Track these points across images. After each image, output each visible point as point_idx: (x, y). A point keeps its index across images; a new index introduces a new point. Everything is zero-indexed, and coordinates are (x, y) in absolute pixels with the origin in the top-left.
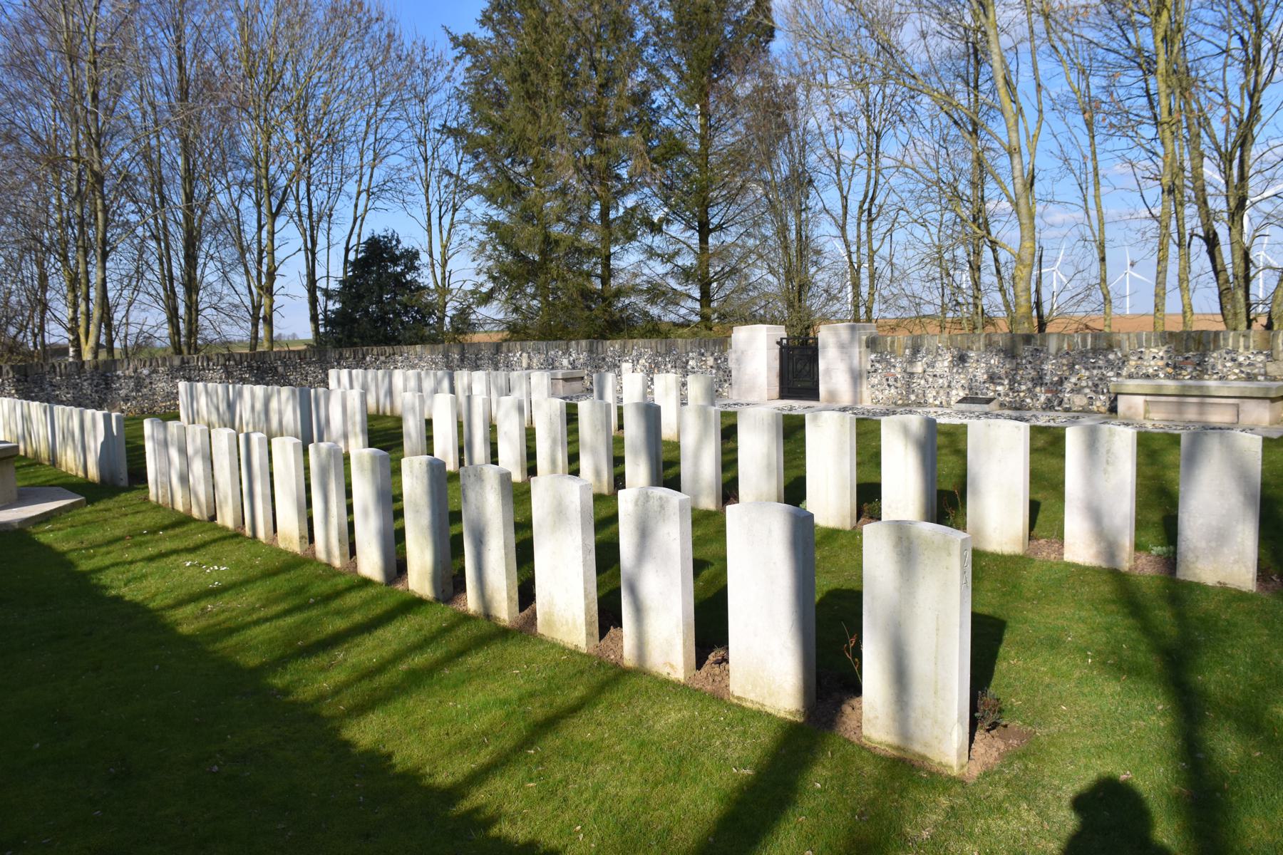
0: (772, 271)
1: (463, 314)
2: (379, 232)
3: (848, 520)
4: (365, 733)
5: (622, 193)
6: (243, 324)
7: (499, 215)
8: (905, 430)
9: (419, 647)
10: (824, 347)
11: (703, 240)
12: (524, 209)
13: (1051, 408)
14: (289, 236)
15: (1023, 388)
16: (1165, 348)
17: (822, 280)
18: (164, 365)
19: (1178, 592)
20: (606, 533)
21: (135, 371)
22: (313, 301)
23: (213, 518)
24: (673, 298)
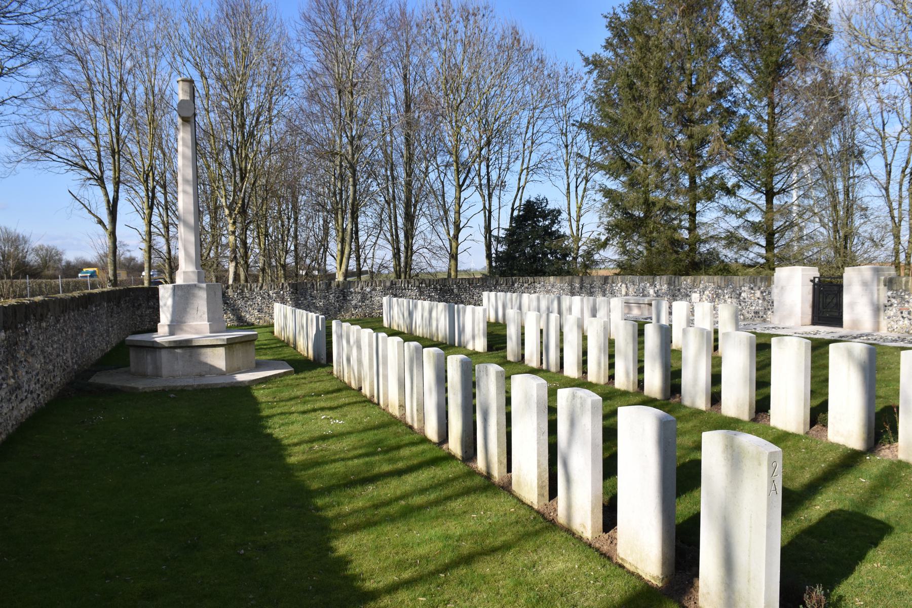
0: (824, 225)
1: (589, 254)
3: (802, 426)
4: (343, 546)
5: (703, 167)
6: (444, 260)
7: (612, 184)
8: (850, 353)
9: (422, 491)
10: (850, 285)
11: (769, 201)
12: (631, 180)
14: (473, 200)
17: (865, 232)
18: (380, 285)
20: (610, 422)
21: (362, 289)
22: (488, 247)
23: (360, 389)
24: (745, 245)
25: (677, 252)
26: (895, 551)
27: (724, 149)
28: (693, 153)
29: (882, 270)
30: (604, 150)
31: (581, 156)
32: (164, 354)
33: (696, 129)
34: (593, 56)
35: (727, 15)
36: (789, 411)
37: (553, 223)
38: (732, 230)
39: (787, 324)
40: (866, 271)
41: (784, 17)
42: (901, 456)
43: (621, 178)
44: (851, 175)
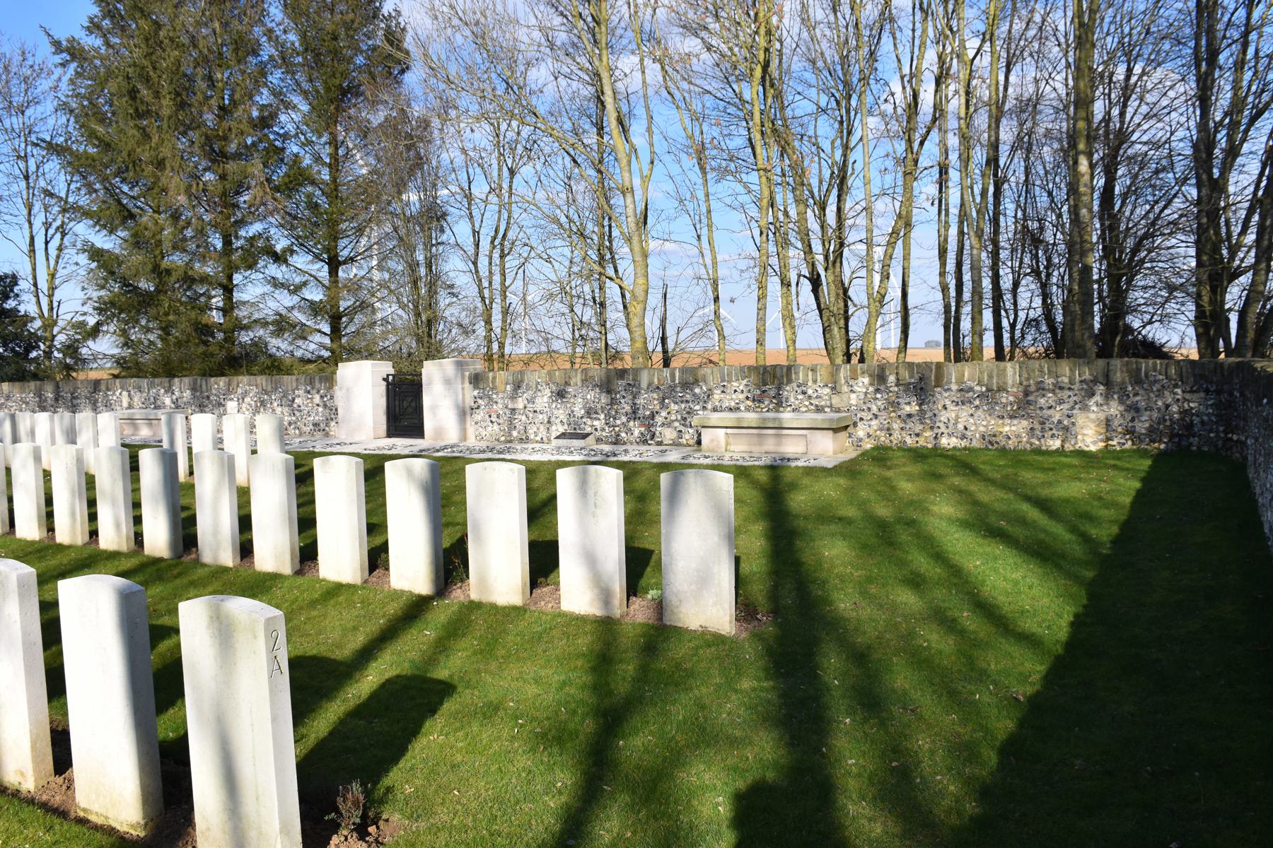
0: (403, 307)
1: (71, 349)
3: (359, 574)
5: (241, 223)
7: (103, 241)
8: (409, 472)
10: (430, 384)
11: (333, 272)
12: (135, 235)
13: (645, 442)
15: (618, 422)
16: (745, 382)
19: (661, 632)
24: (302, 333)
25: (206, 343)
26: (455, 715)
27: (269, 197)
28: (227, 201)
29: (467, 364)
30: (91, 190)
31: (51, 195)
33: (231, 166)
34: (68, 41)
35: (276, 12)
36: (340, 559)
38: (284, 312)
39: (356, 439)
40: (448, 365)
41: (349, 26)
42: (474, 596)
43: (119, 233)
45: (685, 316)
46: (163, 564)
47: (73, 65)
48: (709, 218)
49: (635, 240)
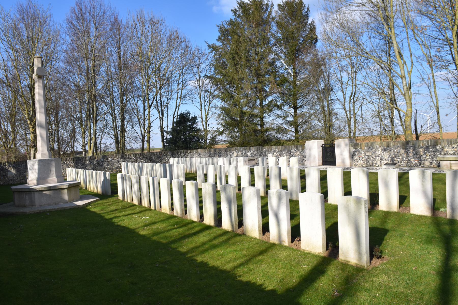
1: (213, 139)
2: (184, 111)
5: (267, 96)
11: (295, 111)
12: (234, 103)
17: (337, 124)
24: (285, 132)
32: (36, 194)
37: (194, 123)
44: (330, 99)
45: (425, 121)
46: (194, 224)
47: (214, 52)
48: (435, 84)
49: (407, 94)
